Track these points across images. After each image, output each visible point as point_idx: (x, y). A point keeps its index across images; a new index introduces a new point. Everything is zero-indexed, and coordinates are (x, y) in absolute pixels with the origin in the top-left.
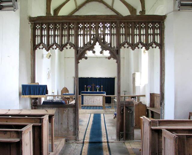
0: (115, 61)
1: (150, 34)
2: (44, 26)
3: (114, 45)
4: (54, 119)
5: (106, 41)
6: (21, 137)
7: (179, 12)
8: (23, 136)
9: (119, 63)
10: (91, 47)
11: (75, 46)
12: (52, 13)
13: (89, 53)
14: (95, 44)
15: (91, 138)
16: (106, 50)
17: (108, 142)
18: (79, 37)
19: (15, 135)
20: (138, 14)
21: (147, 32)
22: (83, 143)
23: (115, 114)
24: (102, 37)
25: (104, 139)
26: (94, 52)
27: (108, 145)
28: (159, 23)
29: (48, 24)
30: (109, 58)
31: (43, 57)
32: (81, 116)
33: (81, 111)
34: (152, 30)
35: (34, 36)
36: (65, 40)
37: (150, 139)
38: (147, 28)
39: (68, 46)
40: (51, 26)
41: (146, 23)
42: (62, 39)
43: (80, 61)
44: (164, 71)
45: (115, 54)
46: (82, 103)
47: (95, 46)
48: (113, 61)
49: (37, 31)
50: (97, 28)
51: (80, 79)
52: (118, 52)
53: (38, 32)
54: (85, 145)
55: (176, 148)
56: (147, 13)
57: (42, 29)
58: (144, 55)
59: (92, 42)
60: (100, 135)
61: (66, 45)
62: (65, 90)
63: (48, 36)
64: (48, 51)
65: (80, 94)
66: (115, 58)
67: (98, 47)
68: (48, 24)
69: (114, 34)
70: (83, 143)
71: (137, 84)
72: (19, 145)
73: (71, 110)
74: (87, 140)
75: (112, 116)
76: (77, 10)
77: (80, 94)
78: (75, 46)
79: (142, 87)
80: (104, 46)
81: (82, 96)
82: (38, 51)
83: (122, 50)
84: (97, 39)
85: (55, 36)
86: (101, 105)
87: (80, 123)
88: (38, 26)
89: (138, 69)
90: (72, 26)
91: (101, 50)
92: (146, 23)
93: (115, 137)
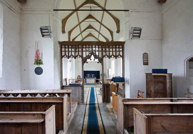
0: (101, 64)
1: (118, 51)
2: (66, 46)
3: (100, 56)
4: (71, 95)
5: (97, 54)
6: (45, 118)
7: (132, 40)
8: (46, 117)
9: (103, 65)
10: (89, 57)
11: (82, 57)
12: (71, 40)
13: (88, 60)
14: (91, 56)
15: (90, 101)
16: (96, 59)
17: (98, 104)
18: (84, 52)
19: (41, 116)
20: (110, 41)
21: (116, 50)
22: (86, 104)
23: (101, 89)
24: (95, 52)
25: (96, 102)
26: (91, 60)
27: (98, 106)
28: (122, 46)
29: (68, 46)
30: (98, 63)
31: (67, 61)
32: (85, 89)
33: (85, 86)
34: (118, 49)
35: (61, 51)
36: (77, 54)
37: (123, 110)
38: (116, 48)
39: (78, 57)
40: (70, 47)
41: (116, 46)
42: (75, 53)
43: (84, 64)
44: (124, 69)
45: (101, 61)
46: (86, 82)
47: (91, 57)
48: (100, 64)
49: (63, 49)
50: (92, 48)
51: (85, 72)
52: (102, 60)
53: (63, 49)
54: (87, 106)
55: (146, 126)
56: (115, 40)
57: (65, 48)
58: (113, 60)
59: (90, 55)
60: (94, 100)
61: (77, 56)
62: (79, 76)
63: (116, 51)
64: (68, 59)
65: (84, 78)
66: (101, 63)
67: (92, 57)
68: (68, 46)
69: (100, 51)
70: (86, 104)
71: (110, 74)
72: (43, 123)
73: (80, 88)
74: (88, 103)
75: (99, 89)
76: (83, 40)
77: (84, 78)
78: (82, 57)
79: (112, 75)
80: (96, 57)
81: (86, 79)
82: (63, 59)
83: (104, 58)
84: (92, 53)
85: (72, 51)
86: (94, 83)
87: (85, 93)
88: (63, 46)
89: (110, 67)
90: (80, 46)
91: (94, 59)
92: (116, 46)
93: (101, 101)
